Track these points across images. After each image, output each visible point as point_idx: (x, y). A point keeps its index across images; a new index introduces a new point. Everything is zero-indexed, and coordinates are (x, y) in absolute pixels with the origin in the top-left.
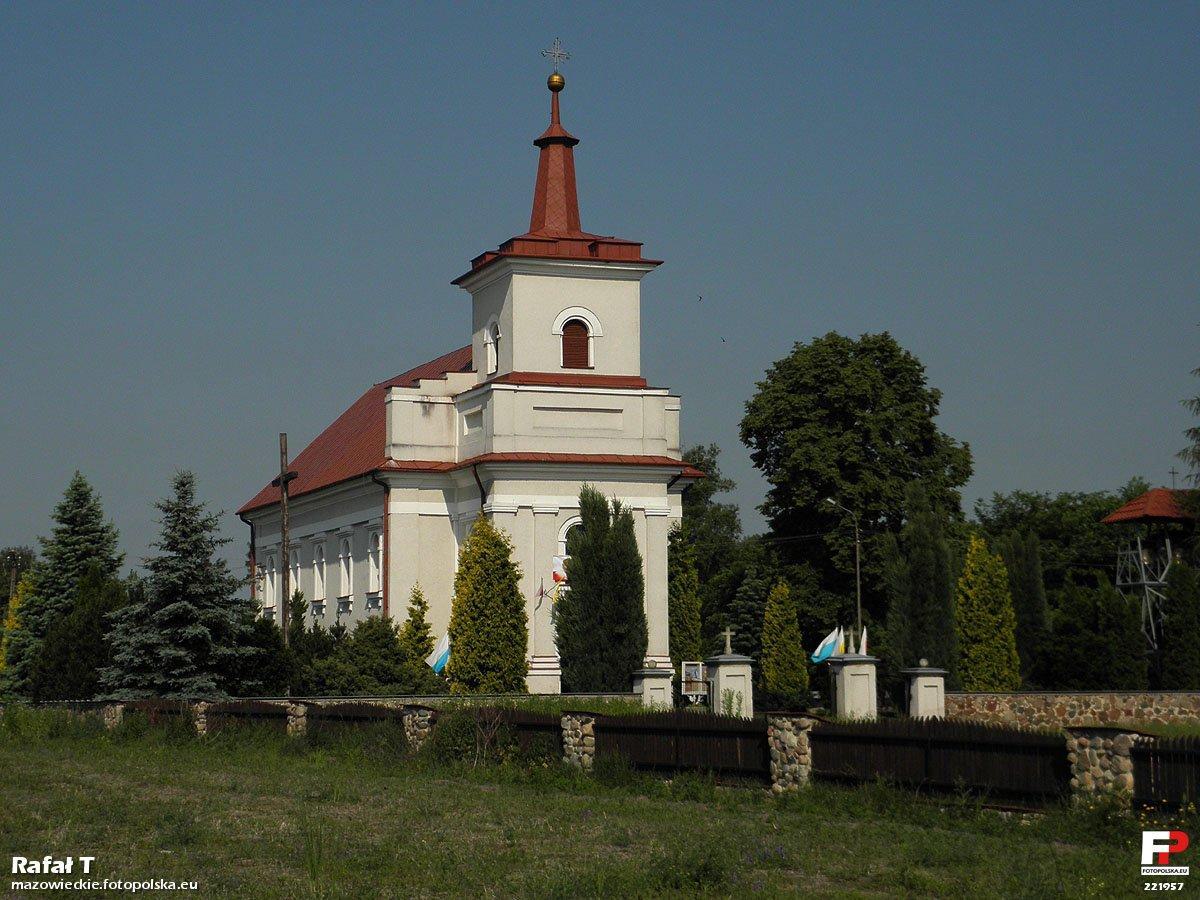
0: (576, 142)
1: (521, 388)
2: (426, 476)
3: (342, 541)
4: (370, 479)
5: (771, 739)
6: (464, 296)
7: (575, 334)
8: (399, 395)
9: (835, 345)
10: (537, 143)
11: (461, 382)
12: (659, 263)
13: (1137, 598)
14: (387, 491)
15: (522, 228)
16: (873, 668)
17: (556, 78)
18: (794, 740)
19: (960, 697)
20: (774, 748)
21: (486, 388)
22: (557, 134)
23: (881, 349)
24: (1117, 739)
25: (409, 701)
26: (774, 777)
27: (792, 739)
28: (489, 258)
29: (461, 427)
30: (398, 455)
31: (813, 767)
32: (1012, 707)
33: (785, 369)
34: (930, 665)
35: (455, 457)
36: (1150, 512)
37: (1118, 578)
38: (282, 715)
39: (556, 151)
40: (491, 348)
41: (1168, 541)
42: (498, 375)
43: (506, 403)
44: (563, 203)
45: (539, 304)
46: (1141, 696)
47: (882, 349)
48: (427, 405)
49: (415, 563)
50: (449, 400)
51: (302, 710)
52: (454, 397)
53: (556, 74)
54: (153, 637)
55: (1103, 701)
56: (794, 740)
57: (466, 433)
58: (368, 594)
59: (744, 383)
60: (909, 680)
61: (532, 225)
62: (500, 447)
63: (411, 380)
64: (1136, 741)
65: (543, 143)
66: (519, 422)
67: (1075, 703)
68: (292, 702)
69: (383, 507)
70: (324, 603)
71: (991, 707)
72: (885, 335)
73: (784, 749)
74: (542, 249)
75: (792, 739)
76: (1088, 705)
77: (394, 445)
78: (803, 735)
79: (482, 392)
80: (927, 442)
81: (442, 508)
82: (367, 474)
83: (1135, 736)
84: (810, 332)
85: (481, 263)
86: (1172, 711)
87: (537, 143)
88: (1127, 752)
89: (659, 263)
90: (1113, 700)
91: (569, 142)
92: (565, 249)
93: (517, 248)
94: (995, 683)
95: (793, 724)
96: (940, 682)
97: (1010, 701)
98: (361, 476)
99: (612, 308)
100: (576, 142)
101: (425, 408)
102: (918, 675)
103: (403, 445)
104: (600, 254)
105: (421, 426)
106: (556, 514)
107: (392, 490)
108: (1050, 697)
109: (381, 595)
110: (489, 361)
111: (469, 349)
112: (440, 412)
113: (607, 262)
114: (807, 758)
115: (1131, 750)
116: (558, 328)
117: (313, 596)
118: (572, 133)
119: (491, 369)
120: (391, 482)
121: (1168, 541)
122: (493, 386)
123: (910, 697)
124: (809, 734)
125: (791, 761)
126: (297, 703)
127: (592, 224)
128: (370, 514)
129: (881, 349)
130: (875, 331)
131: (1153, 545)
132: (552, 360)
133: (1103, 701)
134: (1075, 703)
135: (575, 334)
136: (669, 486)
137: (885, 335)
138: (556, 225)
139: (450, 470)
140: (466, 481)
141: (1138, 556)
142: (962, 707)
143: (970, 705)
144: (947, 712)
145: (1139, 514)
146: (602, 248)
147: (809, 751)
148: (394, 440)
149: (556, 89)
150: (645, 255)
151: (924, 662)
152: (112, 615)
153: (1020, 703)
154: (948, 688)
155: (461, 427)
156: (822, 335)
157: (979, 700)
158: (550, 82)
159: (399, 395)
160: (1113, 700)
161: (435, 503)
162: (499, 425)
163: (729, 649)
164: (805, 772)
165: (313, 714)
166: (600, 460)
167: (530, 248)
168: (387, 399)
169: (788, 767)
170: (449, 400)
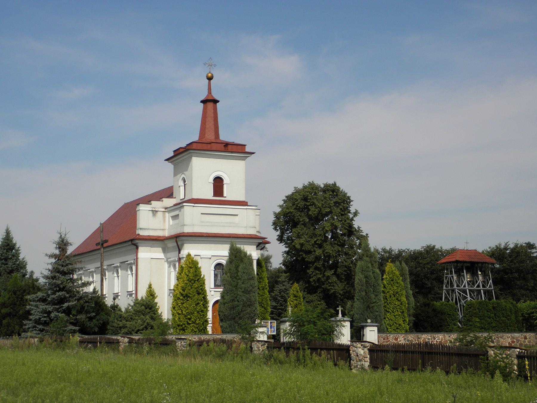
0: (218, 101)
1: (196, 205)
2: (154, 242)
3: (115, 269)
4: (130, 243)
5: (351, 352)
6: (170, 166)
7: (218, 182)
8: (143, 208)
9: (312, 188)
10: (202, 102)
11: (169, 202)
12: (253, 153)
13: (382, 294)
14: (137, 248)
15: (196, 138)
16: (349, 323)
17: (210, 75)
18: (362, 352)
19: (384, 335)
20: (353, 355)
21: (181, 205)
22: (210, 98)
23: (333, 191)
24: (511, 351)
25: (177, 337)
26: (353, 367)
27: (361, 351)
28: (181, 150)
29: (169, 221)
30: (142, 233)
31: (370, 363)
32: (405, 339)
33: (290, 199)
34: (372, 322)
35: (167, 234)
36: (458, 259)
37: (444, 286)
38: (118, 342)
39: (210, 105)
40: (182, 188)
41: (465, 271)
42: (186, 199)
43: (189, 210)
44: (213, 127)
45: (203, 169)
46: (456, 334)
47: (332, 190)
48: (154, 212)
49: (152, 276)
50: (164, 210)
51: (126, 340)
52: (166, 208)
53: (210, 73)
54: (50, 308)
55: (441, 337)
56: (362, 352)
57: (171, 224)
58: (128, 292)
59: (275, 203)
60: (363, 328)
61: (200, 136)
62: (187, 230)
63: (147, 200)
64: (519, 352)
65: (204, 102)
66: (194, 219)
67: (430, 337)
68: (122, 337)
69: (135, 255)
70: (119, 294)
71: (396, 339)
72: (335, 184)
73: (357, 355)
74: (205, 146)
75: (361, 351)
76: (435, 339)
77: (140, 229)
78: (366, 350)
79: (179, 206)
80: (351, 231)
81: (161, 255)
82: (129, 241)
83: (518, 350)
84: (300, 182)
85: (178, 152)
86: (528, 339)
87: (202, 102)
88: (515, 356)
89: (253, 153)
90: (444, 336)
91: (215, 102)
92: (214, 146)
93: (194, 146)
94: (397, 329)
95: (362, 345)
96: (376, 329)
97: (404, 337)
98: (126, 242)
99: (231, 170)
100: (218, 101)
101: (153, 213)
102: (367, 326)
103: (148, 229)
104: (235, 150)
105: (151, 221)
106: (210, 258)
107: (140, 248)
108: (420, 335)
109: (134, 292)
110: (180, 194)
111: (171, 188)
112: (160, 215)
113: (232, 152)
114: (368, 359)
115: (517, 355)
116: (211, 180)
117: (114, 290)
118: (217, 98)
119: (182, 197)
120: (139, 244)
121: (465, 271)
122: (184, 204)
123: (363, 335)
124: (368, 349)
125: (360, 361)
126: (124, 337)
127: (224, 136)
128: (130, 259)
129: (333, 191)
130: (331, 182)
131: (459, 272)
132: (209, 194)
133: (441, 337)
134: (430, 337)
135: (218, 182)
136: (257, 247)
137: (335, 184)
138: (210, 136)
139: (165, 239)
140: (172, 244)
141: (452, 277)
142: (384, 339)
143: (388, 339)
144: (378, 341)
145: (454, 260)
146: (230, 147)
147: (368, 356)
148: (141, 226)
149: (210, 79)
150: (247, 149)
151: (369, 321)
152: (28, 297)
153: (408, 337)
154: (379, 331)
155: (169, 221)
156: (306, 184)
157: (391, 336)
158: (207, 76)
159: (143, 208)
160: (444, 336)
161: (157, 253)
162: (187, 221)
163: (340, 315)
164: (367, 364)
165: (131, 341)
166: (228, 236)
167: (200, 146)
168: (137, 209)
169: (359, 363)
170: (164, 210)
